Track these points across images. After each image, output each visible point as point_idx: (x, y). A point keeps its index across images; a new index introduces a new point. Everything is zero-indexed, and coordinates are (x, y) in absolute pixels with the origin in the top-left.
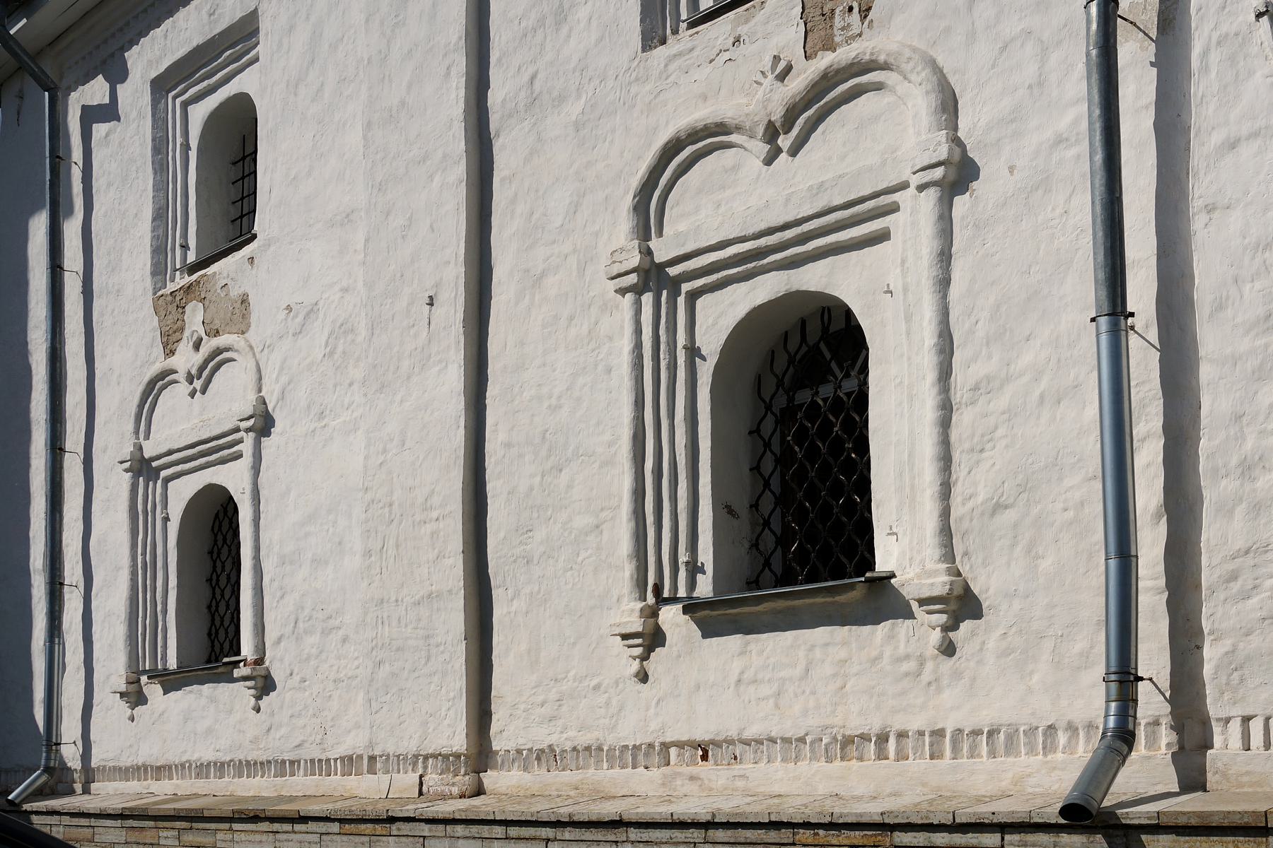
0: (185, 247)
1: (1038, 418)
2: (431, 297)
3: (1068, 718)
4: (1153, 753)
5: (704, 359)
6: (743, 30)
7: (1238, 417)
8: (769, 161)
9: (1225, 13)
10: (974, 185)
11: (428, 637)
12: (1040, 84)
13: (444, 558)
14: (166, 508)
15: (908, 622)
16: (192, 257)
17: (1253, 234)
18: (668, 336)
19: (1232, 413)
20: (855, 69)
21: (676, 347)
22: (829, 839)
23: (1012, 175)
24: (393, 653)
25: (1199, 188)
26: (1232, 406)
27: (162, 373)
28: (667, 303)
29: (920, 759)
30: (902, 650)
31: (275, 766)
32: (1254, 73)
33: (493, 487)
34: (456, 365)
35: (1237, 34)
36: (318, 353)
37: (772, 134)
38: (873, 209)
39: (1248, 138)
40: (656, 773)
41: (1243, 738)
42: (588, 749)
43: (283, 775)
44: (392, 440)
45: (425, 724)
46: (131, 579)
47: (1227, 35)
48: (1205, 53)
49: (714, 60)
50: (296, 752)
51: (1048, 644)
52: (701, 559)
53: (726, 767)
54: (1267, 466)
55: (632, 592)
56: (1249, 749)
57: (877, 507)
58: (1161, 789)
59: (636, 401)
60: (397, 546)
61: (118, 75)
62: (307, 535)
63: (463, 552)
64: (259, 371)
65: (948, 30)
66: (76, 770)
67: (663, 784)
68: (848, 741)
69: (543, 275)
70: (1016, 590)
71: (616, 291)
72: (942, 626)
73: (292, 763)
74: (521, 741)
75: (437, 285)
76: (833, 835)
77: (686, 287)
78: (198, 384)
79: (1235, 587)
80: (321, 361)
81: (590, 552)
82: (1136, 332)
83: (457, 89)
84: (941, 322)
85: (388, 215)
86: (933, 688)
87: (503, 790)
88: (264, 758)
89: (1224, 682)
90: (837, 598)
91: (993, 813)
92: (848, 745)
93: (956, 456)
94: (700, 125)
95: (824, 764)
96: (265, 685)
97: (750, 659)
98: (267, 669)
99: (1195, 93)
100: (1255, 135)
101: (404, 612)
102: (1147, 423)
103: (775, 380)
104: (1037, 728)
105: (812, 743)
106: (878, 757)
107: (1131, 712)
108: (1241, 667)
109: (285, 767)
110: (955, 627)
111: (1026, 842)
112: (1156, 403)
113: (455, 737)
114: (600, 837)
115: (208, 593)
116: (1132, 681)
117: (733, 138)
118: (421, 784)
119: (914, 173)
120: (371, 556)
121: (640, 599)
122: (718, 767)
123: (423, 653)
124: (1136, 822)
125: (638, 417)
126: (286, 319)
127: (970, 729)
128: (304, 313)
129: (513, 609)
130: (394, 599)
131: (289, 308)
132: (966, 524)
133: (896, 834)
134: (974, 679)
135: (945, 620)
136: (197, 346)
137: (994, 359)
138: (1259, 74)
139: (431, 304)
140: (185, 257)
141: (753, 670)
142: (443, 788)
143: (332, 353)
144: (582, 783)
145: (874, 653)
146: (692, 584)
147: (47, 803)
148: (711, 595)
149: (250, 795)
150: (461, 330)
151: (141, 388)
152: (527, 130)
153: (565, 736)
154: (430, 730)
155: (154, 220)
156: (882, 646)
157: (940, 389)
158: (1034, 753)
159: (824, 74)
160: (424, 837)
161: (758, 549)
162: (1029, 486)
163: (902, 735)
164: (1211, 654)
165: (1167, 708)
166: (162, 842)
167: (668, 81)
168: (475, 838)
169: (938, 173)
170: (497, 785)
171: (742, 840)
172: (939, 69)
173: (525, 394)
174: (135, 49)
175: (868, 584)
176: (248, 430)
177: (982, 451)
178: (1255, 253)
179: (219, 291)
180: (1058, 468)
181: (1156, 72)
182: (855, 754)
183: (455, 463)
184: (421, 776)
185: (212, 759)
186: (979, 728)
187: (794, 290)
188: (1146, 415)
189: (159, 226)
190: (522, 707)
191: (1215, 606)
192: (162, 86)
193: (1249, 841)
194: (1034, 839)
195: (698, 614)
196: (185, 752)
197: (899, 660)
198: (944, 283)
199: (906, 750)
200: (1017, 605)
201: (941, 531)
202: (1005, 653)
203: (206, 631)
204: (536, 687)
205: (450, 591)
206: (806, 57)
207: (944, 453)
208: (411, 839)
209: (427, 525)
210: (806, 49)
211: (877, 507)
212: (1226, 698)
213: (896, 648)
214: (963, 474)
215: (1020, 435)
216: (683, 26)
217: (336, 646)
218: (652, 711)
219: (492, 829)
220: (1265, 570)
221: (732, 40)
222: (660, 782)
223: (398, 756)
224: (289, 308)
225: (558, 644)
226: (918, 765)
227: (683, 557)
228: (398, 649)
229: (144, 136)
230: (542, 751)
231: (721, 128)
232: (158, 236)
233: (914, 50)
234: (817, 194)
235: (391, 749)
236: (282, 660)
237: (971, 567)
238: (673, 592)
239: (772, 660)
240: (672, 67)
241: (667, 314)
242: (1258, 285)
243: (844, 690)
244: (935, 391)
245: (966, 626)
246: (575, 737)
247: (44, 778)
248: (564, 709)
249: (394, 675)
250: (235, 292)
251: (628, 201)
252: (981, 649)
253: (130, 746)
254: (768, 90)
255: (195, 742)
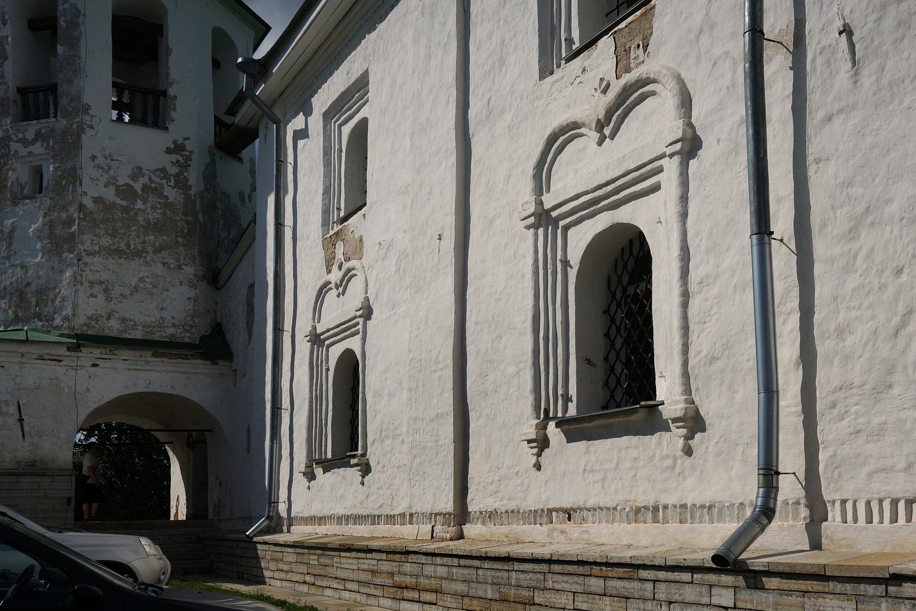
0: (339, 209)
1: (734, 301)
2: (440, 235)
3: (751, 498)
4: (796, 523)
5: (572, 268)
6: (586, 64)
7: (835, 298)
8: (600, 143)
9: (824, 32)
10: (700, 152)
11: (437, 441)
12: (733, 86)
13: (445, 392)
14: (328, 363)
15: (668, 434)
16: (342, 214)
17: (841, 176)
18: (552, 254)
19: (831, 295)
20: (640, 84)
21: (557, 260)
22: (608, 573)
23: (719, 145)
24: (421, 451)
25: (811, 148)
26: (832, 291)
27: (325, 283)
28: (551, 234)
29: (675, 523)
30: (664, 452)
31: (371, 518)
32: (840, 71)
33: (470, 349)
34: (451, 276)
35: (830, 46)
36: (393, 270)
37: (600, 126)
38: (650, 170)
39: (837, 114)
40: (545, 528)
41: (842, 514)
42: (513, 511)
43: (341, 525)
44: (421, 321)
45: (435, 494)
46: (309, 405)
47: (825, 46)
48: (814, 60)
49: (573, 83)
50: (380, 510)
51: (740, 449)
52: (570, 393)
53: (578, 525)
54: (851, 330)
55: (532, 414)
56: (847, 523)
57: (657, 359)
58: (799, 548)
59: (534, 295)
60: (424, 385)
61: (308, 113)
62: (386, 379)
63: (453, 389)
64: (366, 281)
65: (687, 55)
66: (285, 518)
67: (548, 535)
68: (638, 511)
69: (493, 219)
70: (723, 413)
71: (524, 228)
72: (684, 436)
73: (378, 516)
74: (482, 506)
75: (442, 228)
76: (610, 570)
77: (562, 223)
78: (341, 289)
79: (835, 412)
80: (394, 274)
81: (515, 388)
82: (784, 243)
83: (452, 110)
84: (682, 241)
85: (421, 187)
86: (681, 477)
87: (472, 536)
88: (365, 514)
89: (830, 476)
90: (630, 418)
91: (685, 560)
92: (637, 513)
93: (691, 326)
94: (565, 124)
95: (626, 525)
96: (366, 470)
97: (590, 456)
98: (368, 459)
99: (809, 86)
100: (841, 111)
101: (426, 426)
102: (791, 303)
103: (617, 279)
104: (734, 505)
105: (621, 510)
106: (654, 521)
107: (773, 496)
108: (839, 466)
109: (374, 519)
110: (692, 438)
111: (704, 579)
112: (796, 289)
113: (447, 504)
114: (501, 567)
115: (351, 412)
116: (772, 475)
117: (583, 130)
118: (433, 531)
119: (667, 147)
120: (411, 391)
121: (536, 418)
122: (576, 525)
123: (434, 450)
124: (757, 568)
125: (536, 305)
126: (378, 250)
127: (700, 505)
128: (386, 246)
129: (479, 424)
130: (421, 418)
131: (380, 244)
132: (696, 371)
133: (640, 571)
134: (702, 472)
135: (685, 433)
136: (340, 268)
137: (711, 263)
138: (842, 71)
139: (440, 239)
140: (339, 214)
141: (591, 464)
142: (443, 534)
143: (399, 269)
144: (510, 533)
145: (651, 454)
146: (565, 409)
147: (264, 537)
148: (576, 415)
149: (359, 535)
150: (453, 254)
151: (315, 293)
152: (487, 131)
153: (502, 503)
154: (437, 498)
155: (323, 194)
156: (655, 449)
157: (682, 284)
158: (733, 521)
159: (624, 88)
160: (423, 564)
161: (608, 386)
162: (729, 345)
163: (665, 507)
164: (823, 456)
165: (802, 493)
166: (311, 562)
167: (551, 98)
168: (445, 565)
169: (678, 146)
170: (470, 533)
171: (567, 572)
172: (682, 80)
173: (485, 293)
174: (316, 96)
175: (648, 409)
176: (360, 316)
177: (705, 323)
178: (843, 189)
179: (350, 235)
180: (744, 333)
181: (792, 74)
182: (642, 519)
183: (450, 334)
184: (433, 527)
185: (343, 513)
186: (704, 504)
187: (615, 222)
188: (790, 298)
189: (326, 198)
190: (482, 484)
191: (824, 425)
192: (328, 116)
193: (819, 584)
194: (708, 578)
195: (563, 428)
196: (331, 509)
197: (663, 458)
198: (684, 215)
199: (668, 517)
200: (723, 424)
201: (683, 375)
202: (719, 454)
203: (349, 436)
204: (489, 472)
205: (447, 413)
206: (617, 78)
207: (685, 324)
208: (417, 565)
209: (437, 373)
210: (617, 73)
211: (657, 359)
212: (831, 487)
213: (662, 451)
214: (695, 338)
215: (723, 312)
216: (563, 62)
217: (399, 446)
218: (543, 489)
219: (452, 560)
220: (851, 401)
221: (581, 70)
222: (547, 534)
223: (423, 514)
224: (380, 244)
225: (499, 446)
226: (673, 527)
227: (560, 392)
228: (423, 448)
229: (320, 145)
230: (491, 512)
231: (575, 125)
232: (326, 203)
233: (668, 69)
234: (622, 162)
235: (419, 510)
236: (374, 454)
237: (700, 398)
238: (555, 414)
239: (601, 457)
240: (554, 88)
241: (551, 240)
242: (845, 210)
243: (636, 478)
244: (679, 285)
245: (698, 436)
246: (507, 504)
247: (266, 523)
248: (502, 486)
249: (421, 464)
250: (357, 235)
251: (530, 172)
252: (706, 452)
253: (308, 504)
254: (597, 100)
255: (336, 502)
